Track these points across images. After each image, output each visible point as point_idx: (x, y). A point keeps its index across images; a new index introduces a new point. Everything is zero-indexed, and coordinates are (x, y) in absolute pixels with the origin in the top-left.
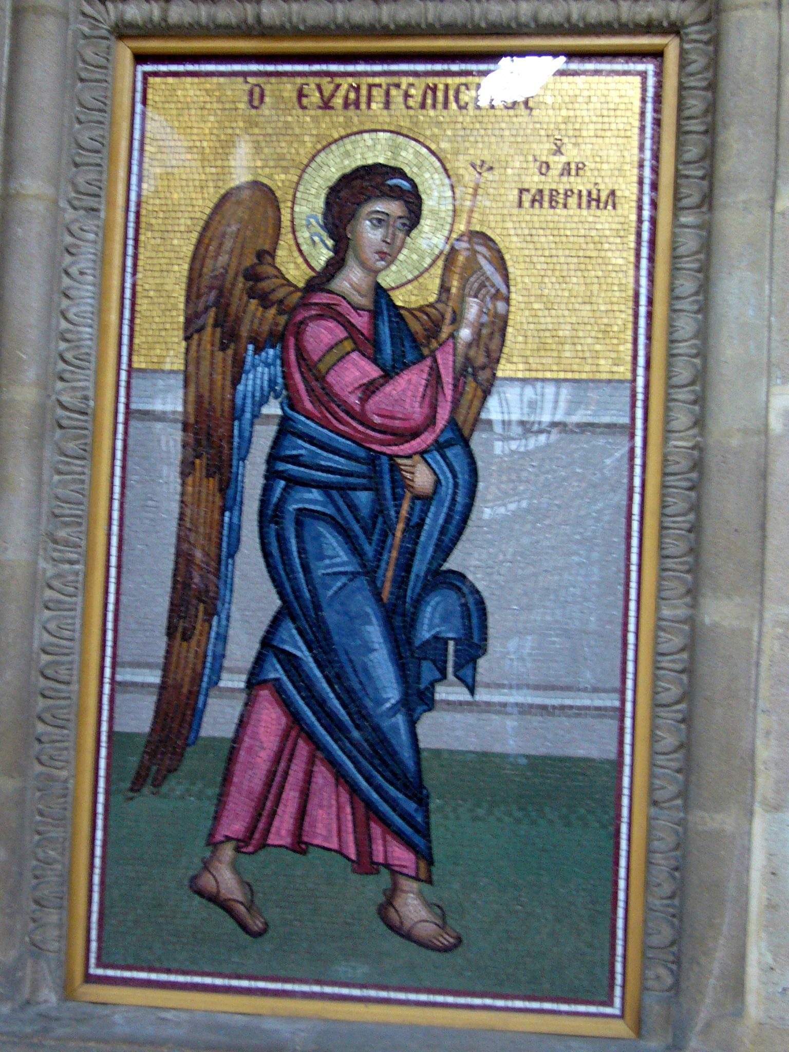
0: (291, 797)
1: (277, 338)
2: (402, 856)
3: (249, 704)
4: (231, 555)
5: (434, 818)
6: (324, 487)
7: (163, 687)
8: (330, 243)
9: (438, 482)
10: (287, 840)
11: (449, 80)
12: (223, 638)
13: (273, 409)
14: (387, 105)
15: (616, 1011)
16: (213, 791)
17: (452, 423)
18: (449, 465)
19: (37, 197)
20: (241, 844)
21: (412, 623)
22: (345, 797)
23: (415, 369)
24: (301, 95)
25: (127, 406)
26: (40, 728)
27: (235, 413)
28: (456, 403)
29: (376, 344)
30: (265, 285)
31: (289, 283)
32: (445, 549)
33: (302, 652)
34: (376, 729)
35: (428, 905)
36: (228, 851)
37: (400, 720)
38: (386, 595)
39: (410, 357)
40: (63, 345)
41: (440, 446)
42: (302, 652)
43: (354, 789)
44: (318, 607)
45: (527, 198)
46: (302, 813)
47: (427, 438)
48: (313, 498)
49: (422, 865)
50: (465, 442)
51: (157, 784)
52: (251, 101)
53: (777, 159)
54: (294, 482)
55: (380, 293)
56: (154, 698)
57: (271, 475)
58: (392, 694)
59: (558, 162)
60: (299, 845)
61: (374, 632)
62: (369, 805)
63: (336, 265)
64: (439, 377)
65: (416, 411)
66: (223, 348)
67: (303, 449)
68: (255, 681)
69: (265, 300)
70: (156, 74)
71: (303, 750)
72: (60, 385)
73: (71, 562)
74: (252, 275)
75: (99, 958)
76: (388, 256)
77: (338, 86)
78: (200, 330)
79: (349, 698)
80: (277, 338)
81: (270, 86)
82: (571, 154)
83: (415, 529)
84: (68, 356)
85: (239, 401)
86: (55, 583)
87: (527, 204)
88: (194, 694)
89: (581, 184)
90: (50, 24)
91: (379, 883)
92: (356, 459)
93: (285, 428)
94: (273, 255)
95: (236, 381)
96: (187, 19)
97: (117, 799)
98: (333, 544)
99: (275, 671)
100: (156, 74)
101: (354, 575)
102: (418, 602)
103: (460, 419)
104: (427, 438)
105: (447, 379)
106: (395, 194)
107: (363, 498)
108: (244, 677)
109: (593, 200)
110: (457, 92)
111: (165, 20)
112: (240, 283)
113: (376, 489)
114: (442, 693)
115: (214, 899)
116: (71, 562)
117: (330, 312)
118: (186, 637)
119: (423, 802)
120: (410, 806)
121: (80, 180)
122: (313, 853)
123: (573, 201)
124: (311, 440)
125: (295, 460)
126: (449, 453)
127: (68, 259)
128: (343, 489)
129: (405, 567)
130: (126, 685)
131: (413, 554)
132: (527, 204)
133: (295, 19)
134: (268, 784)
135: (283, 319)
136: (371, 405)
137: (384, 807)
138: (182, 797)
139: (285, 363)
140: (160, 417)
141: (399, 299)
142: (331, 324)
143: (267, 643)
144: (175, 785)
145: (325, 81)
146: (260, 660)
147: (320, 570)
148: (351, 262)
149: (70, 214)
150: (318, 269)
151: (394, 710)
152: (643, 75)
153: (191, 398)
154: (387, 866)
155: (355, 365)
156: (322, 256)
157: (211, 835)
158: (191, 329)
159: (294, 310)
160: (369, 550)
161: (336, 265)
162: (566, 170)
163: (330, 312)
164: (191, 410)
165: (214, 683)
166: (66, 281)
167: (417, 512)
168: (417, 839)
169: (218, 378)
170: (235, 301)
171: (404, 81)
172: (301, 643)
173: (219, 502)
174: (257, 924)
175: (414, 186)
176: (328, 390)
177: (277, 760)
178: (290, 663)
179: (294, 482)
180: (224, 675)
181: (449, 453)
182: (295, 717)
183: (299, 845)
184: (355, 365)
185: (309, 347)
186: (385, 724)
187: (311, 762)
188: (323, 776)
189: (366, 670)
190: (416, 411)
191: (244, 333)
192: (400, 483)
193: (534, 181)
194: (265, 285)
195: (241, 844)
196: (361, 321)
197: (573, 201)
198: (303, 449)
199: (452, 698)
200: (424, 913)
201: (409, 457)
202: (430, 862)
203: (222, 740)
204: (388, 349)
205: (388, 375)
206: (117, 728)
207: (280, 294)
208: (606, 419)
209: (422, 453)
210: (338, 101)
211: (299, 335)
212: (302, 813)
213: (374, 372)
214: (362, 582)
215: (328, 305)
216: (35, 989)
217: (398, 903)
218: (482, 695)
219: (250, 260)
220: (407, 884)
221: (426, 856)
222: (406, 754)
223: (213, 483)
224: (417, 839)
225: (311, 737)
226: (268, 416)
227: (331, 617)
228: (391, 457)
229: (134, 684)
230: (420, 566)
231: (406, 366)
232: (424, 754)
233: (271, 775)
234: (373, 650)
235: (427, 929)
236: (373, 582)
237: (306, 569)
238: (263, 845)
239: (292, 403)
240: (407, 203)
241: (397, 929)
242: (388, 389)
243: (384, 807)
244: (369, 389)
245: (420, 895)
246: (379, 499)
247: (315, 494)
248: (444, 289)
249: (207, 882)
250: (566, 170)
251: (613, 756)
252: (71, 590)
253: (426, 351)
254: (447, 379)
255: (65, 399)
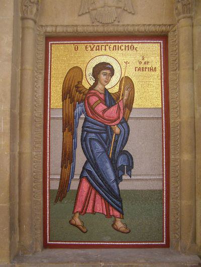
0: (91, 202)
1: (83, 100)
2: (117, 213)
3: (81, 182)
4: (75, 149)
5: (124, 205)
6: (94, 133)
7: (61, 179)
8: (94, 79)
9: (121, 131)
10: (91, 212)
11: (119, 44)
12: (74, 168)
13: (83, 116)
14: (105, 50)
15: (164, 243)
16: (73, 201)
17: (123, 118)
18: (123, 127)
19: (29, 69)
20: (80, 213)
21: (116, 162)
22: (103, 201)
23: (114, 106)
24: (86, 48)
25: (50, 116)
26: (34, 190)
27: (75, 117)
28: (124, 115)
29: (105, 101)
30: (80, 89)
31: (85, 88)
32: (123, 145)
33: (92, 170)
34: (109, 186)
35: (123, 224)
36: (77, 214)
37: (115, 184)
38: (110, 156)
39: (113, 104)
40: (35, 103)
41: (121, 123)
42: (92, 170)
43: (105, 199)
44: (95, 160)
45: (137, 69)
46: (93, 207)
47: (118, 122)
48: (93, 136)
49: (121, 215)
50: (126, 122)
51: (61, 201)
52: (75, 49)
53: (193, 58)
54: (88, 132)
55: (106, 90)
56: (59, 182)
57: (83, 131)
58: (113, 178)
59: (143, 62)
60: (93, 212)
61: (108, 165)
62: (109, 203)
63: (95, 84)
64: (120, 108)
65: (115, 115)
66: (71, 103)
67: (90, 125)
68: (81, 177)
69: (80, 93)
70: (53, 44)
71: (93, 192)
72: (35, 112)
73: (39, 152)
74: (77, 87)
75: (49, 239)
76: (107, 82)
77: (94, 46)
78: (66, 99)
79: (103, 179)
80: (83, 100)
81: (79, 46)
82: (146, 60)
83: (116, 141)
84: (36, 105)
85: (75, 115)
86: (36, 157)
87: (137, 71)
88: (68, 180)
89: (149, 66)
90: (31, 31)
91: (111, 220)
92: (103, 127)
93: (86, 120)
94: (81, 82)
95: (74, 110)
96: (61, 31)
97: (51, 204)
98: (98, 145)
99: (86, 174)
100: (53, 44)
101: (103, 153)
102: (118, 157)
103: (125, 118)
104: (118, 122)
105: (122, 108)
106: (109, 69)
107: (104, 135)
108: (79, 176)
109: (151, 69)
110: (121, 47)
111: (56, 31)
112: (74, 89)
113: (107, 133)
114: (124, 177)
115: (75, 225)
116: (39, 152)
117: (95, 94)
118: (66, 168)
119: (121, 201)
120: (118, 203)
121: (38, 66)
122: (96, 214)
123: (147, 70)
124: (92, 123)
125: (87, 127)
126: (123, 125)
127: (36, 84)
128: (100, 133)
129: (114, 150)
130: (52, 179)
131: (116, 147)
132: (137, 71)
133: (85, 31)
134: (86, 200)
135: (84, 96)
136: (105, 114)
137: (112, 203)
138: (66, 203)
139: (85, 106)
140: (58, 118)
141: (110, 91)
142: (95, 97)
143: (84, 168)
144: (65, 201)
145: (91, 45)
146: (82, 172)
147: (95, 152)
148: (99, 84)
149: (36, 74)
150: (92, 85)
151: (113, 182)
152: (160, 43)
153: (64, 114)
154: (113, 216)
155: (101, 106)
156: (92, 82)
157: (73, 211)
158: (64, 99)
159: (86, 95)
160: (106, 147)
161: (95, 84)
162: (145, 63)
163: (95, 94)
164: (64, 117)
165: (72, 178)
166: (36, 89)
167: (116, 138)
168: (120, 209)
169: (70, 110)
170: (73, 93)
171: (109, 45)
172: (92, 168)
173: (72, 137)
174: (85, 230)
175: (112, 67)
176: (96, 113)
177: (88, 194)
178: (90, 172)
179: (88, 132)
180: (75, 176)
181: (123, 125)
182: (91, 184)
183: (93, 212)
184: (101, 106)
185: (91, 102)
186: (112, 185)
187: (95, 195)
188: (98, 197)
189: (107, 173)
190: (115, 115)
191: (76, 99)
192: (112, 131)
193: (138, 65)
194: (80, 89)
195: (80, 213)
196: (102, 96)
197: (147, 70)
198: (90, 125)
199: (126, 178)
200: (122, 226)
201: (114, 126)
202: (123, 214)
203: (74, 190)
204: (108, 102)
205: (109, 107)
206: (51, 189)
207: (83, 91)
208: (151, 116)
209: (117, 125)
210: (95, 49)
211: (88, 99)
212: (93, 207)
213: (105, 107)
214: (105, 154)
215: (95, 93)
216: (36, 249)
217: (116, 224)
218: (133, 177)
219: (76, 84)
220: (118, 220)
221: (122, 213)
222: (117, 191)
223: (70, 133)
224: (120, 209)
225: (95, 188)
226: (82, 118)
227: (98, 162)
228: (110, 126)
229: (54, 179)
230: (118, 149)
231: (112, 106)
232: (121, 191)
233: (87, 197)
234: (108, 169)
235: (123, 229)
236: (107, 154)
237: (92, 151)
238: (85, 213)
239: (87, 114)
240: (111, 71)
241: (118, 230)
242: (109, 111)
243: (112, 203)
244: (104, 111)
245: (121, 221)
246: (108, 135)
247: (93, 135)
248: (120, 89)
249: (73, 222)
250: (145, 63)
251: (161, 189)
252: (39, 158)
253: (117, 102)
254: (122, 108)
255: (36, 115)
